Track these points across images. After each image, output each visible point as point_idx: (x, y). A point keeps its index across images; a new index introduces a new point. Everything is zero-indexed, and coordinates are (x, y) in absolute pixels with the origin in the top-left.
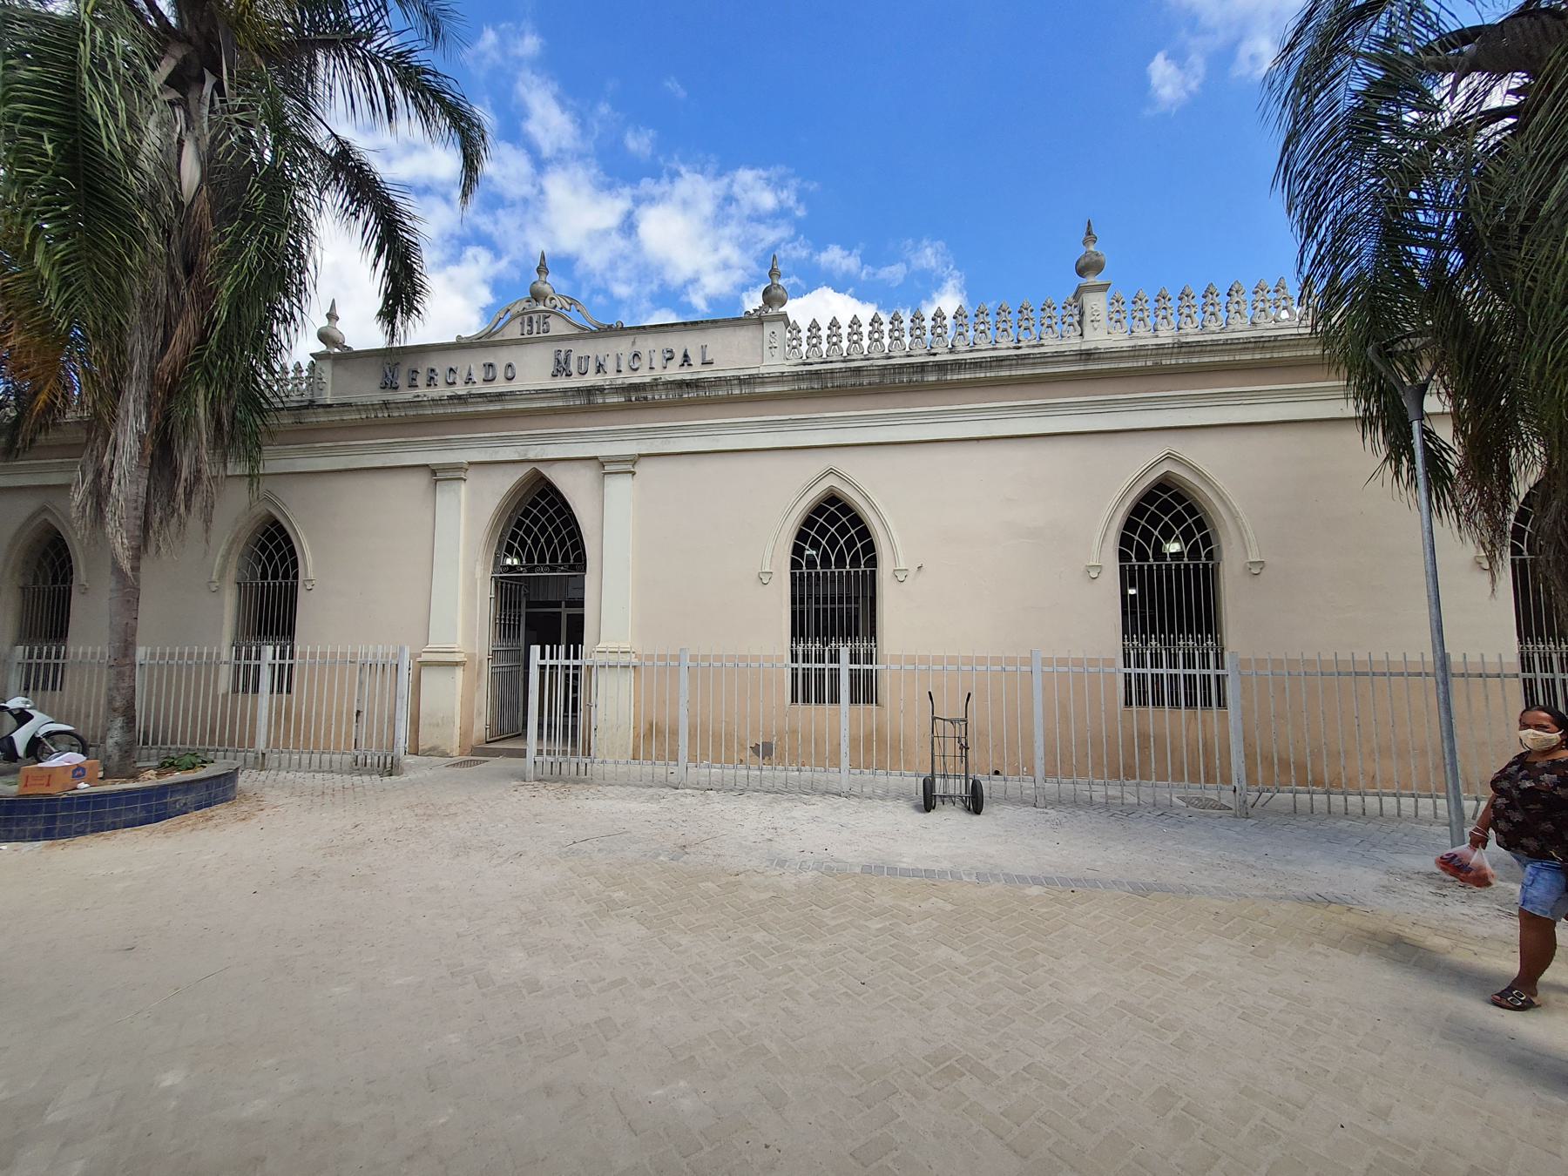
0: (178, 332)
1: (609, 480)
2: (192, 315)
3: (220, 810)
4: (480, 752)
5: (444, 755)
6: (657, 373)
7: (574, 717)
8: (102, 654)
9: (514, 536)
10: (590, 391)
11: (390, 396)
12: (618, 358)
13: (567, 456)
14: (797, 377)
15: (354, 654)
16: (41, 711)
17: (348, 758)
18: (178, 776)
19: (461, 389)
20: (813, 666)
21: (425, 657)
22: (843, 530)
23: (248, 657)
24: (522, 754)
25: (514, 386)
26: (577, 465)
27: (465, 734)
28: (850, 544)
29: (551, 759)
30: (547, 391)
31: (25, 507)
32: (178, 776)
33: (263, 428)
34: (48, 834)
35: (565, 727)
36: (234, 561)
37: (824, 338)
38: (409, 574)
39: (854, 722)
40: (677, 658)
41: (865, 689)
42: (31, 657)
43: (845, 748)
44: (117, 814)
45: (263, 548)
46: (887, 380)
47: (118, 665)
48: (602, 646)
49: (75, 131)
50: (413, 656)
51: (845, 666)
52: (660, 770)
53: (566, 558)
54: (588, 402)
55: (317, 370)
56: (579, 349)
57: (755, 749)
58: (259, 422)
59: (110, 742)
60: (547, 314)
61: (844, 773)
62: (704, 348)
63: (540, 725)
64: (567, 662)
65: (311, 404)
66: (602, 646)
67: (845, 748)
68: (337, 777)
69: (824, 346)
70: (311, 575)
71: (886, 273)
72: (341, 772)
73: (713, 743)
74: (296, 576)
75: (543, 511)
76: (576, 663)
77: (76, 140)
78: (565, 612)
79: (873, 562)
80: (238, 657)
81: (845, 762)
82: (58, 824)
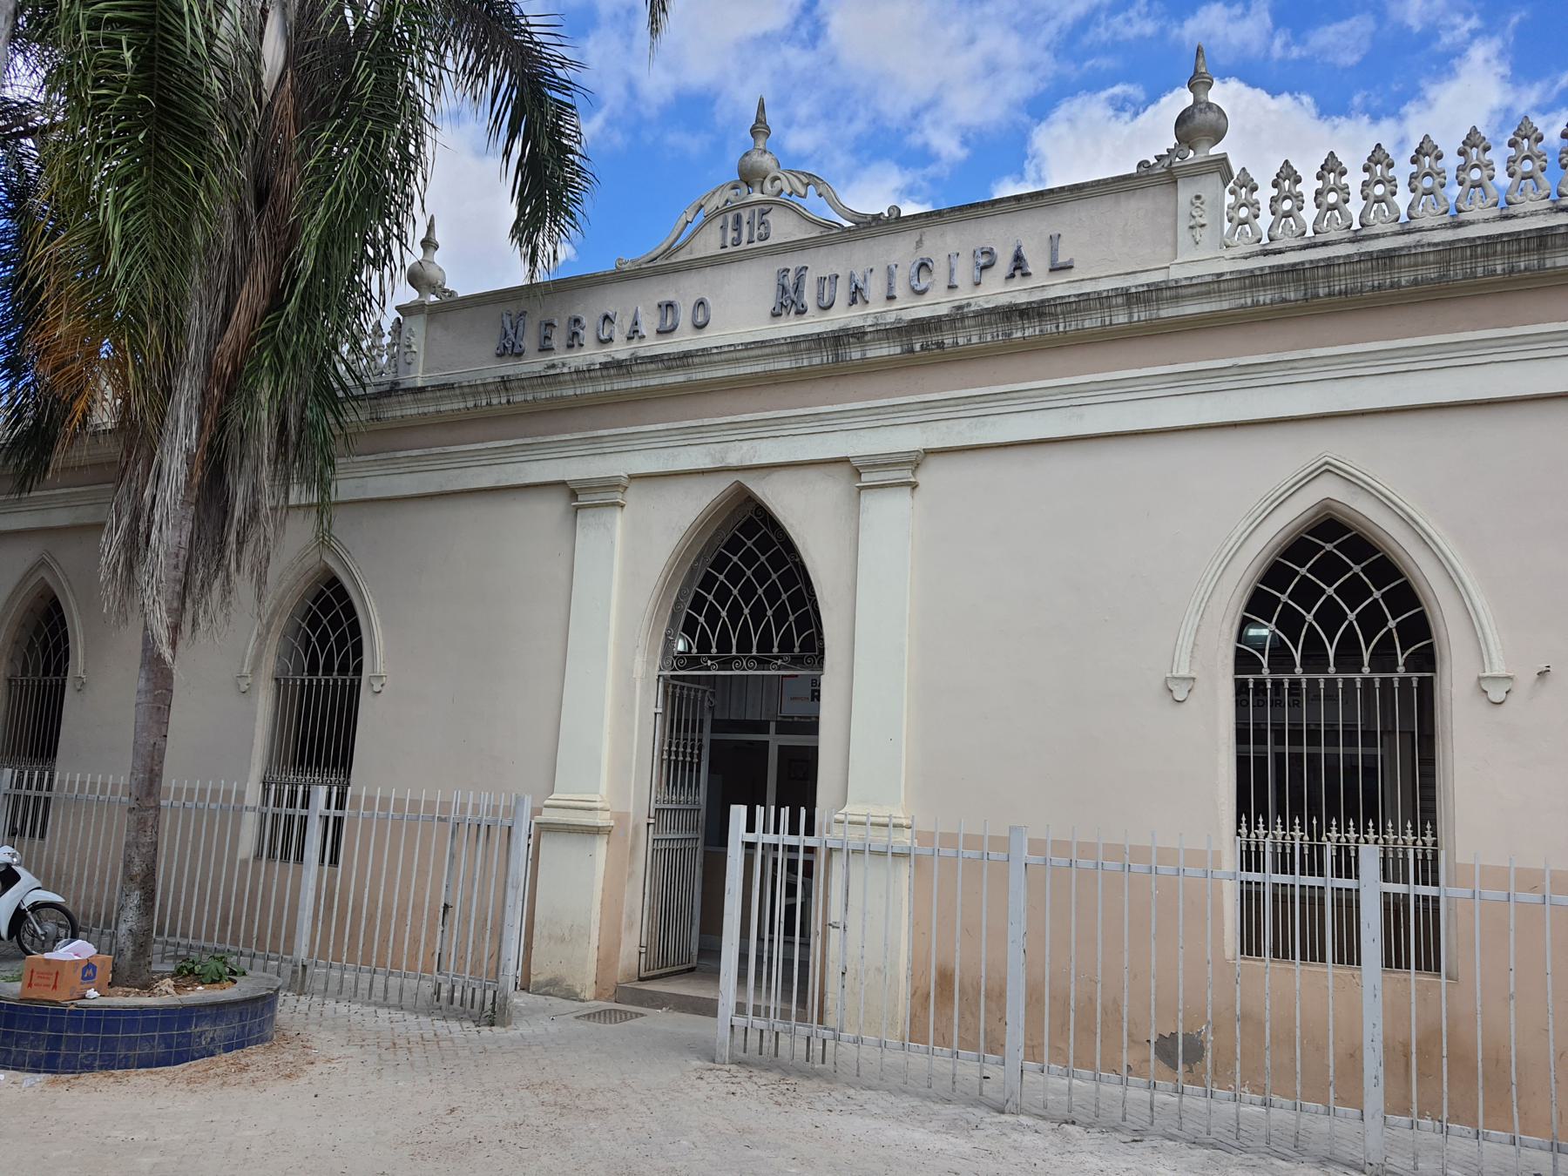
0: (244, 295)
1: (870, 501)
2: (261, 270)
3: (254, 1055)
4: (629, 996)
5: (571, 995)
6: (960, 296)
7: (805, 945)
8: (115, 786)
9: (698, 603)
10: (838, 339)
11: (510, 368)
12: (890, 274)
13: (794, 461)
14: (1251, 280)
15: (446, 806)
16: (28, 868)
17: (427, 988)
18: (199, 994)
19: (621, 350)
20: (1298, 880)
21: (548, 816)
22: (1354, 592)
23: (292, 804)
24: (708, 1008)
25: (710, 338)
26: (811, 473)
27: (606, 960)
28: (1372, 620)
29: (760, 1023)
30: (762, 344)
31: (19, 559)
32: (199, 994)
33: (337, 432)
34: (48, 1064)
35: (788, 963)
36: (273, 642)
37: (1309, 197)
38: (549, 671)
39: (1395, 1012)
40: (1001, 843)
41: (1416, 939)
42: (19, 786)
43: (1373, 1063)
44: (131, 1043)
45: (314, 623)
46: (1456, 272)
47: (141, 809)
48: (853, 809)
49: (153, 26)
50: (537, 811)
51: (1371, 888)
52: (968, 1068)
53: (786, 645)
54: (835, 359)
55: (405, 333)
56: (820, 264)
57: (1165, 1048)
58: (332, 421)
59: (123, 928)
60: (765, 207)
61: (1373, 1123)
62: (1054, 240)
63: (743, 957)
64: (793, 840)
65: (394, 390)
66: (853, 809)
67: (1373, 1063)
68: (411, 1018)
69: (1309, 213)
70: (380, 669)
71: (1326, 36)
72: (415, 1010)
73: (1076, 1027)
74: (358, 669)
75: (749, 559)
76: (810, 841)
77: (153, 40)
78: (775, 741)
79: (1426, 660)
80: (265, 802)
81: (1374, 1097)
82: (63, 1051)
